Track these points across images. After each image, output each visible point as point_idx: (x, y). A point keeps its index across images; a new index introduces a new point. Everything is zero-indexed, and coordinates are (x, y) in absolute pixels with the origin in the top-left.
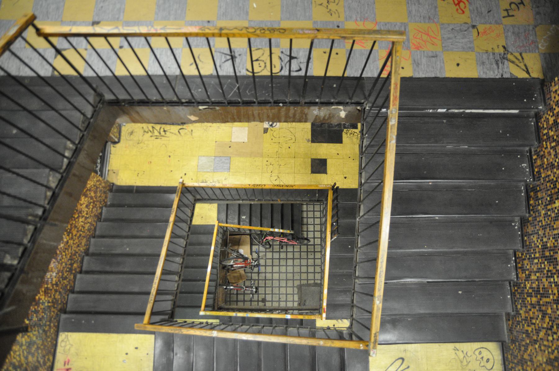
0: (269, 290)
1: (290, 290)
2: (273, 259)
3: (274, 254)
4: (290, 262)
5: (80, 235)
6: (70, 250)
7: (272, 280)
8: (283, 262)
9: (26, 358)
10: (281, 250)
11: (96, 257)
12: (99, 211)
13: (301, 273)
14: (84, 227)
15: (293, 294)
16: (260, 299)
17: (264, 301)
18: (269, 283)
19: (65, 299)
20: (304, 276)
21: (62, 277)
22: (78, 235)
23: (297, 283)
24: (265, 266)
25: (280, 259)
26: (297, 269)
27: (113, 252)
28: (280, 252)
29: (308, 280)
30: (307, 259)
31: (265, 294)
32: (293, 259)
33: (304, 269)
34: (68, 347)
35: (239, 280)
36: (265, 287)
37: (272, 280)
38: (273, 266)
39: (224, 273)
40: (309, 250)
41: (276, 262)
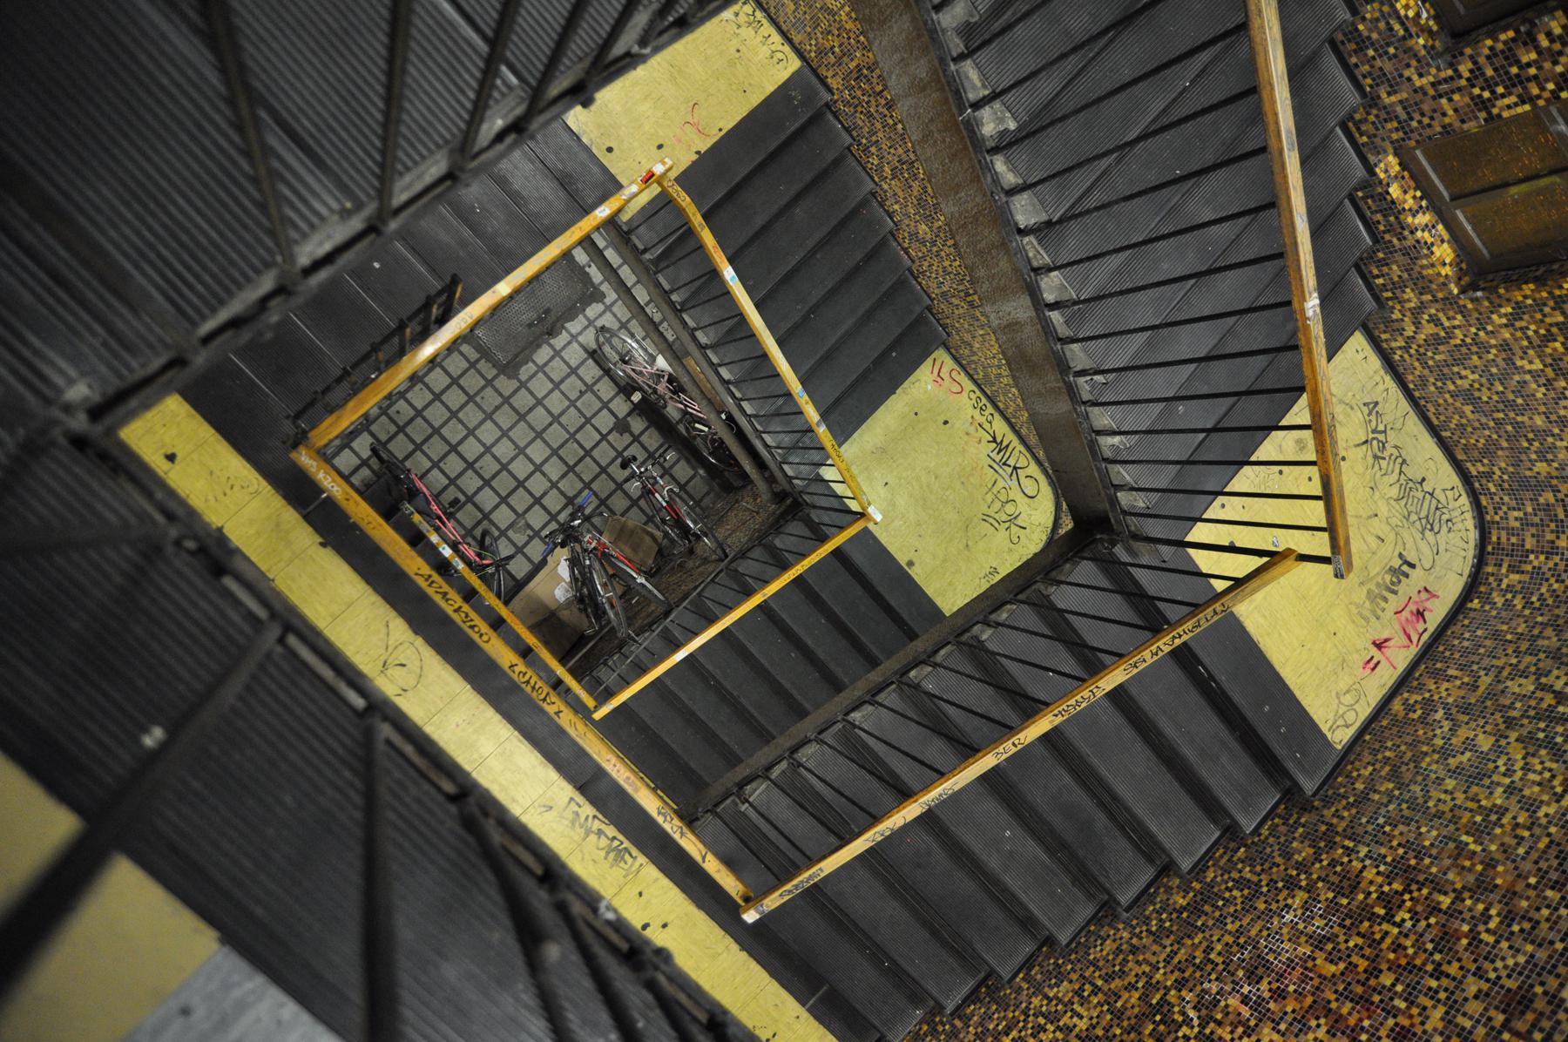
0: (589, 437)
1: (540, 386)
2: (504, 500)
3: (487, 508)
4: (471, 449)
5: (1108, 978)
6: (1182, 955)
7: (555, 452)
8: (488, 466)
9: (1498, 750)
10: (463, 499)
11: (1102, 880)
12: (976, 1011)
13: (471, 399)
14: (1078, 993)
15: (541, 368)
16: (627, 438)
17: (621, 426)
18: (572, 453)
19: (1273, 828)
20: (472, 382)
21: (1256, 894)
22: (1116, 984)
23: (506, 385)
24: (538, 501)
25: (487, 483)
26: (472, 415)
27: (1044, 856)
28: (470, 499)
29: (473, 365)
30: (419, 413)
31: (604, 437)
32: (454, 448)
33: (454, 398)
34: (1348, 699)
35: (632, 532)
36: (588, 453)
37: (555, 452)
38: (521, 484)
39: (680, 570)
40: (393, 429)
41: (504, 484)
